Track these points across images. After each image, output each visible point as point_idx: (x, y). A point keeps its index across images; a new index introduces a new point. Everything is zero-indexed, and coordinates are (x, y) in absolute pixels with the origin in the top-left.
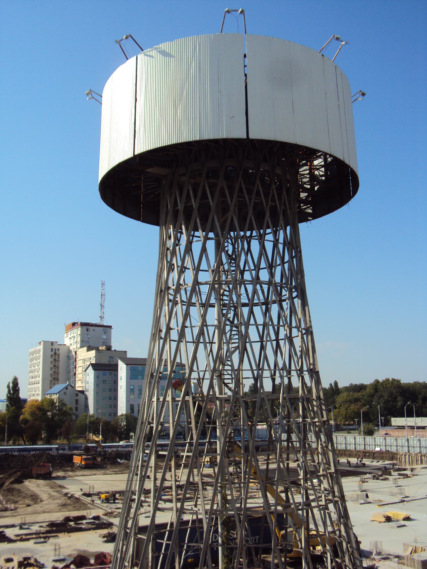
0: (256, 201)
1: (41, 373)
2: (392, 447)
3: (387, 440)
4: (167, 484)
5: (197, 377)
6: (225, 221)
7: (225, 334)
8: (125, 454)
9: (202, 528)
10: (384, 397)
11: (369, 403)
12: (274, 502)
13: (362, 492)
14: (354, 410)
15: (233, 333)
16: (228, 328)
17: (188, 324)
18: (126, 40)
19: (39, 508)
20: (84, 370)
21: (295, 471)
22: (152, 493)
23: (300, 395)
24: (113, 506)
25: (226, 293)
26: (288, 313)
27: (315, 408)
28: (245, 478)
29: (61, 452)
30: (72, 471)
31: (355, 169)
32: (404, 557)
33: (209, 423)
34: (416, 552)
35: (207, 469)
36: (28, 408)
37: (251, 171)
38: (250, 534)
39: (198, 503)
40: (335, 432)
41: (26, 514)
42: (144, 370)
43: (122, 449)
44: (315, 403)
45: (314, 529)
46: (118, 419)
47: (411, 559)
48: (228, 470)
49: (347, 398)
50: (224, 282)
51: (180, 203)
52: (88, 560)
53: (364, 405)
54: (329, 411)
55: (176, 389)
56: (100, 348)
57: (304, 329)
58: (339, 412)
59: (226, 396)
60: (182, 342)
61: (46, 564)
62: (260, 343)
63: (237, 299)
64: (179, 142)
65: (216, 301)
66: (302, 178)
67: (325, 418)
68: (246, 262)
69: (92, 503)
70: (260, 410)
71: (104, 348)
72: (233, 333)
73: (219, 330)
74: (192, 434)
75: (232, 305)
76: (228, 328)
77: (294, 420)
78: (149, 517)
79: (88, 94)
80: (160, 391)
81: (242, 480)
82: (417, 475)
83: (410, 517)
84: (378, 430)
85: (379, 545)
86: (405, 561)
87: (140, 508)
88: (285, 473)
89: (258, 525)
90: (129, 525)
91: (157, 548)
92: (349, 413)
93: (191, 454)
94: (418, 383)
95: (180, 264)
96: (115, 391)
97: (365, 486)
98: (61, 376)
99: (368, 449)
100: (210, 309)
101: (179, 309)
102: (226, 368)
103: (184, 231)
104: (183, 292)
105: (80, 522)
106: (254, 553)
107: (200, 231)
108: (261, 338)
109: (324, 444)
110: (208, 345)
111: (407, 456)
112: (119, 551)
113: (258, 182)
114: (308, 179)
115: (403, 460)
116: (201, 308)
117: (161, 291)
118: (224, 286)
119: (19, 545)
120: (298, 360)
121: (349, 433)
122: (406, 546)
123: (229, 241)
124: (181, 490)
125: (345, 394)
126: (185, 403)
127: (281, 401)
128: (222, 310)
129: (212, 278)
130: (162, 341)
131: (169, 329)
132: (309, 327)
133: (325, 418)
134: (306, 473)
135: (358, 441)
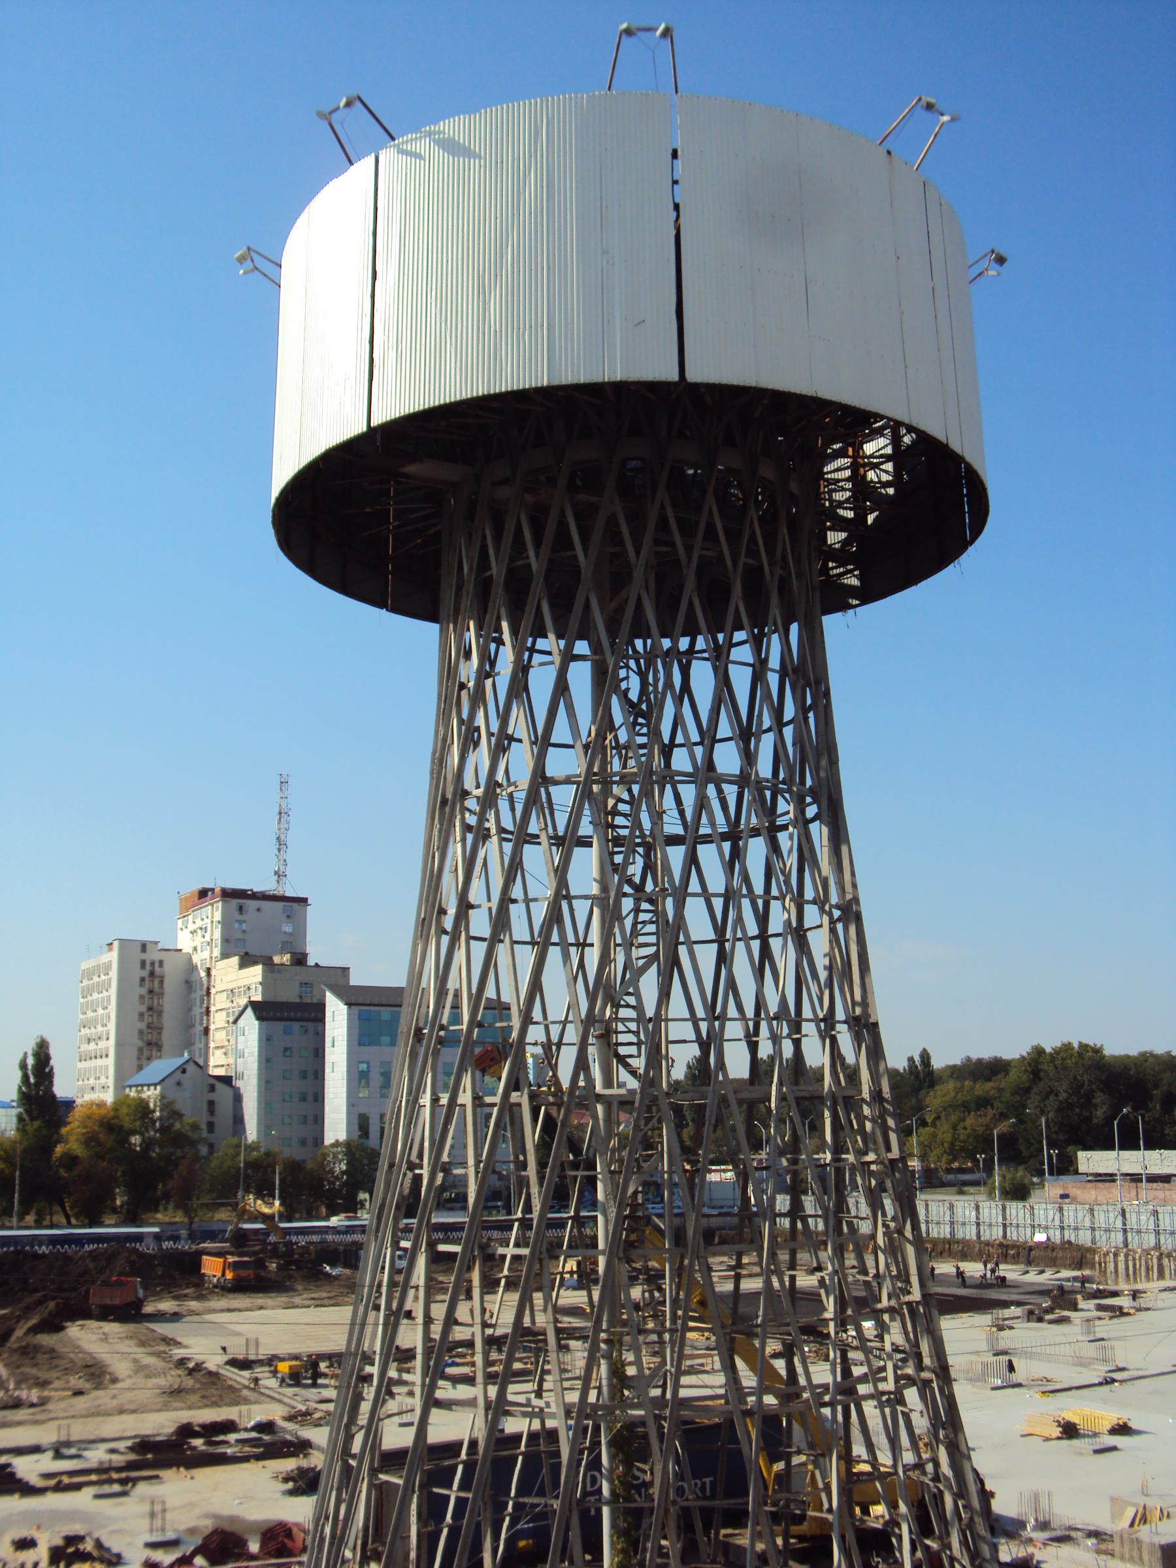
0: (705, 553)
1: (112, 1027)
2: (1081, 1232)
3: (1065, 1213)
4: (459, 1334)
5: (542, 1038)
6: (620, 610)
7: (621, 919)
8: (345, 1250)
9: (558, 1454)
10: (1056, 1095)
11: (1017, 1109)
12: (754, 1384)
13: (996, 1355)
14: (974, 1130)
15: (643, 917)
16: (627, 904)
17: (517, 892)
18: (347, 111)
19: (107, 1400)
20: (231, 1020)
21: (813, 1299)
22: (419, 1358)
23: (826, 1089)
24: (312, 1393)
25: (623, 807)
26: (792, 861)
27: (868, 1126)
28: (674, 1317)
29: (167, 1245)
30: (200, 1297)
31: (976, 466)
32: (1111, 1536)
33: (575, 1166)
34: (1145, 1522)
35: (570, 1293)
36: (76, 1123)
37: (691, 472)
38: (688, 1472)
39: (546, 1386)
40: (921, 1189)
41: (73, 1417)
42: (396, 1020)
43: (337, 1238)
44: (867, 1111)
45: (865, 1456)
46: (325, 1155)
47: (1132, 1541)
48: (628, 1295)
49: (955, 1097)
50: (617, 778)
51: (497, 558)
52: (243, 1543)
53: (1003, 1116)
54: (905, 1133)
55: (484, 1072)
56: (277, 959)
57: (837, 907)
58: (934, 1135)
59: (623, 1091)
60: (501, 941)
61: (127, 1555)
62: (715, 945)
63: (654, 824)
64: (492, 392)
65: (595, 830)
66: (831, 492)
67: (895, 1153)
68: (678, 721)
69: (252, 1386)
70: (715, 1131)
71: (286, 959)
72: (643, 917)
73: (604, 908)
74: (529, 1196)
75: (638, 840)
76: (627, 904)
77: (809, 1156)
78: (411, 1424)
79: (241, 260)
80: (440, 1076)
81: (668, 1324)
82: (1149, 1309)
83: (1130, 1424)
84: (1042, 1185)
85: (1044, 1502)
86: (1116, 1546)
87: (384, 1401)
88: (786, 1303)
89: (710, 1446)
90: (356, 1447)
91: (433, 1509)
92: (962, 1138)
93: (525, 1251)
94: (1152, 1055)
95: (495, 728)
96: (316, 1077)
97: (1006, 1339)
98: (168, 1037)
99: (1015, 1238)
100: (578, 851)
101: (493, 852)
102: (624, 1013)
103: (506, 636)
104: (503, 805)
105: (221, 1438)
106: (699, 1525)
107: (552, 636)
108: (720, 930)
109: (892, 1225)
110: (573, 950)
111: (1121, 1258)
112: (327, 1518)
113: (711, 501)
114: (848, 494)
115: (1111, 1267)
116: (554, 848)
117: (444, 802)
118: (616, 789)
119: (53, 1501)
120: (822, 993)
121: (961, 1193)
122: (1117, 1503)
123: (632, 663)
124: (500, 1351)
125: (951, 1085)
126: (510, 1110)
127: (773, 1106)
128: (613, 854)
129: (585, 766)
130: (445, 939)
131: (465, 906)
132: (850, 901)
133: (895, 1153)
134: (842, 1304)
135: (986, 1214)
